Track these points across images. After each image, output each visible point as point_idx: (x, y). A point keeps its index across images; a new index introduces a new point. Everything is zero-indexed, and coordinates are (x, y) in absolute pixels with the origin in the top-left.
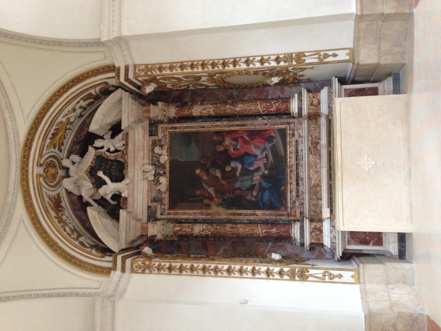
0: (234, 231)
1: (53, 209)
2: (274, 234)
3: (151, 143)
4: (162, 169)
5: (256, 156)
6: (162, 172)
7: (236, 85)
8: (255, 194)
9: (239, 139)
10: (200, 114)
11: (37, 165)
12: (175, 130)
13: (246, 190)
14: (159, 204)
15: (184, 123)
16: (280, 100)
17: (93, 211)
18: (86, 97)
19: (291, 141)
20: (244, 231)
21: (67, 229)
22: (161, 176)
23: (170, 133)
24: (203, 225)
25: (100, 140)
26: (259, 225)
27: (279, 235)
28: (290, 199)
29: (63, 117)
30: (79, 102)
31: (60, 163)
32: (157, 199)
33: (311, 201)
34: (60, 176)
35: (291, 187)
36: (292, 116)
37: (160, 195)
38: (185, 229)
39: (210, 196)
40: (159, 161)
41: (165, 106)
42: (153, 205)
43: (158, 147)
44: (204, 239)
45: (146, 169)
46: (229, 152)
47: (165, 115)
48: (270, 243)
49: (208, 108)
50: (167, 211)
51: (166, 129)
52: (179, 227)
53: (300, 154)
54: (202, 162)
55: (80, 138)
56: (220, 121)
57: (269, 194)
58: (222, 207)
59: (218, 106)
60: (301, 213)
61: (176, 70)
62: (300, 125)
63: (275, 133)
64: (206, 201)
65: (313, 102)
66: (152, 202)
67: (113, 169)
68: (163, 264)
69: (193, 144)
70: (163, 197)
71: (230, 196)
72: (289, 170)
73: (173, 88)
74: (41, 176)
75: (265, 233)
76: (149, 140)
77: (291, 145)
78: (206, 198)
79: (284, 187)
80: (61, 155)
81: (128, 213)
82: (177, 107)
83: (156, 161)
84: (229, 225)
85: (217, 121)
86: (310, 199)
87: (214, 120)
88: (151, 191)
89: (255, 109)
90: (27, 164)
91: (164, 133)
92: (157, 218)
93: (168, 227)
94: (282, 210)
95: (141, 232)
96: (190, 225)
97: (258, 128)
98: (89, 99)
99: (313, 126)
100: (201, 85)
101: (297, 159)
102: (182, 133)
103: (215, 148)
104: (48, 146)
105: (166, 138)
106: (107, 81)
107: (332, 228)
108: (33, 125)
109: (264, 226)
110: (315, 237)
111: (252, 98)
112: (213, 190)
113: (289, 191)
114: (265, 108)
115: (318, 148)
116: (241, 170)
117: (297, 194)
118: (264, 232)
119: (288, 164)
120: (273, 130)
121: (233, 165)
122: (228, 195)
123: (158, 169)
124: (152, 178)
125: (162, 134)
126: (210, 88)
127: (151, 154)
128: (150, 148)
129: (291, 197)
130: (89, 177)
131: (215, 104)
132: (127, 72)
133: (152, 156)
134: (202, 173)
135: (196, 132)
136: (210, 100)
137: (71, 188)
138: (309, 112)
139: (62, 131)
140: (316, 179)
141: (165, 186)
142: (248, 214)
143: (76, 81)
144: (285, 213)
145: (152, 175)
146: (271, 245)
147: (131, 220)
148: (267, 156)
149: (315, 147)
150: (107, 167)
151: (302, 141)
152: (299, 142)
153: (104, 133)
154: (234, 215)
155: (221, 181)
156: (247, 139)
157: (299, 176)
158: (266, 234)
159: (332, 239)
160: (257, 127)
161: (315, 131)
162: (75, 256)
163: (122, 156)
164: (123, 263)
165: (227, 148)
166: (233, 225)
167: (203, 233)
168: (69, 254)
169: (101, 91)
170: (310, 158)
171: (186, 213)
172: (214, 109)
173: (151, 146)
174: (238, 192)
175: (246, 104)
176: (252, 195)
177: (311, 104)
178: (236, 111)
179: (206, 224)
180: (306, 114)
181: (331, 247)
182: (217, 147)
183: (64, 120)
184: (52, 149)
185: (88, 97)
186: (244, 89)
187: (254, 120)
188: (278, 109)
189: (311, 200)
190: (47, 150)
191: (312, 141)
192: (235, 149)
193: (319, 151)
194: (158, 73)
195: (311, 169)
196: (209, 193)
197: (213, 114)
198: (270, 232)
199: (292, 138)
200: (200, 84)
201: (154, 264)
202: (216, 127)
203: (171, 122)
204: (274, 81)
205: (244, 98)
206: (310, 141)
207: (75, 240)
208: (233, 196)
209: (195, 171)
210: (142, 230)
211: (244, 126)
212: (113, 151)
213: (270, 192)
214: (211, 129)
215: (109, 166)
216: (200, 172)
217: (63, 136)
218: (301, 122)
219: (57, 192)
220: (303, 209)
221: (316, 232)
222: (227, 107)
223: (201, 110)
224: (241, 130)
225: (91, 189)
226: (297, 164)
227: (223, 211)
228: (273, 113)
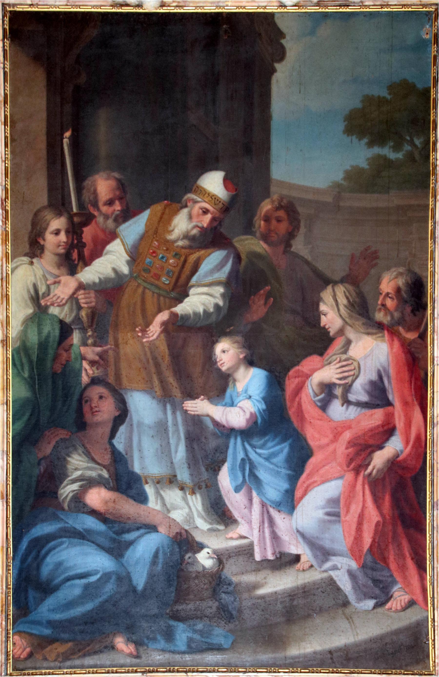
13: (112, 446)
39: (86, 252)
44: (408, 138)
46: (315, 359)
57: (96, 572)
63: (404, 609)
71: (85, 364)
103: (335, 283)
116: (216, 424)
121: (247, 379)
155: (164, 316)
182: (340, 290)
208: (85, 379)
209: (216, 169)
213: (106, 577)
216: (213, 198)
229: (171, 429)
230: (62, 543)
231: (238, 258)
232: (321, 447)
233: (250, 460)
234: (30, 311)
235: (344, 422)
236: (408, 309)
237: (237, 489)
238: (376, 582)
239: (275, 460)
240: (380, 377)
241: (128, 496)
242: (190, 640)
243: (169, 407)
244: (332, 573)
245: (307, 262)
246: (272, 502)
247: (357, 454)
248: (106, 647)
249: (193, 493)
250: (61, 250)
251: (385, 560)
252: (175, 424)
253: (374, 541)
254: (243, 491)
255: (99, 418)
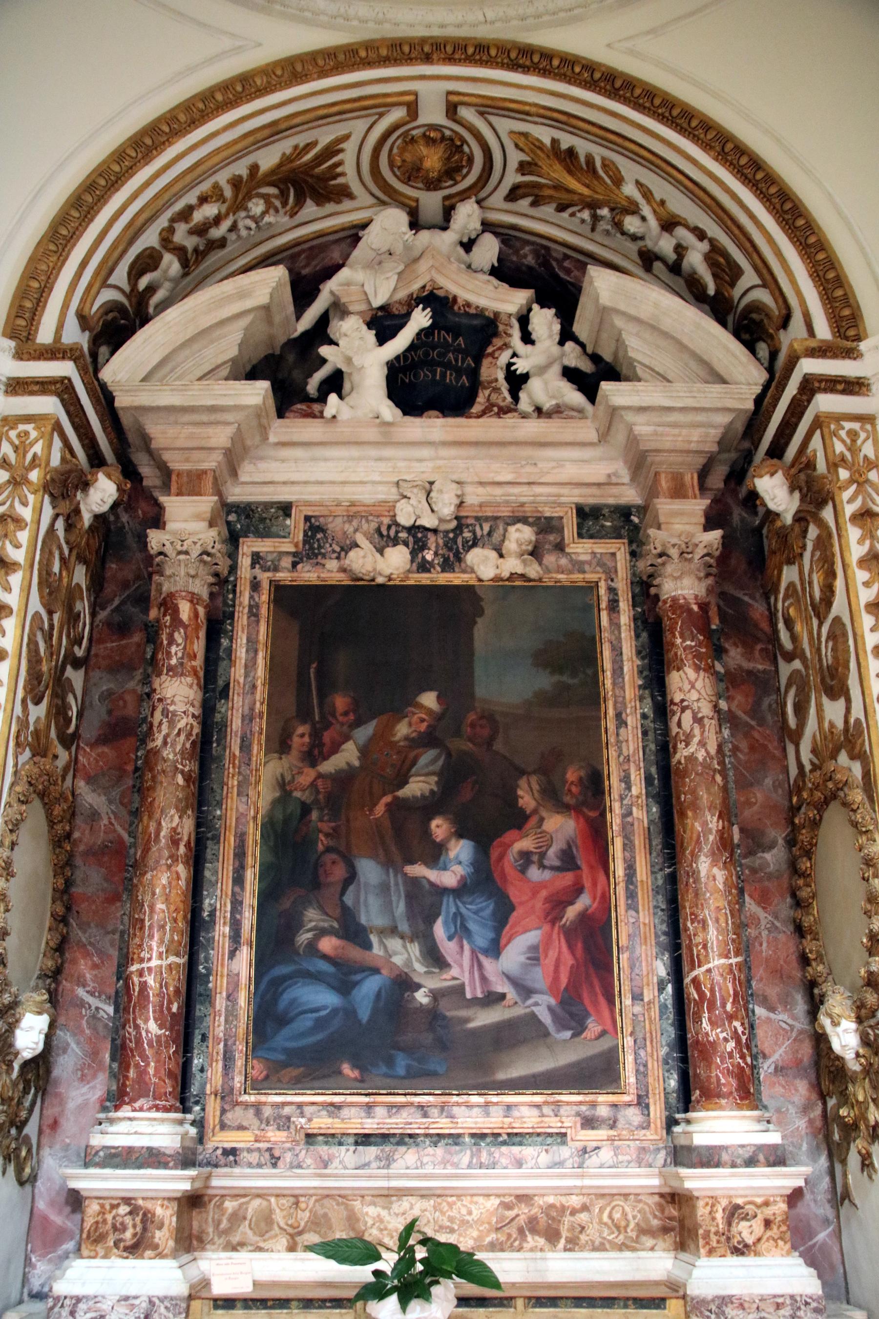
0: (161, 848)
1: (286, 160)
2: (137, 1027)
3: (548, 514)
4: (443, 556)
5: (495, 949)
6: (429, 556)
7: (810, 859)
8: (327, 944)
9: (568, 878)
10: (676, 704)
11: (449, 93)
12: (603, 605)
13: (342, 901)
14: (296, 545)
15: (634, 643)
16: (749, 1060)
17: (270, 290)
18: (721, 260)
19: (564, 1111)
20: (154, 894)
21: (210, 210)
22: (414, 554)
23: (592, 588)
24: (194, 716)
25: (557, 327)
26: (182, 960)
27: (132, 1051)
28: (300, 1106)
29: (638, 183)
30: (701, 235)
31: (463, 196)
32: (318, 540)
33: (283, 1201)
34: (417, 200)
35: (353, 1110)
36: (678, 1116)
37: (334, 551)
38: (180, 641)
39: (325, 750)
40: (475, 544)
41: (708, 555)
42: (295, 525)
43: (533, 538)
45: (441, 491)
47: (668, 556)
48: (110, 1010)
49: (702, 733)
50: (265, 577)
51: (611, 574)
52: (190, 619)
53: (502, 1154)
54: (472, 717)
55: (561, 267)
56: (648, 795)
57: (324, 1007)
58: (275, 803)
59: (713, 778)
60: (233, 1152)
61: (867, 584)
62: (634, 1156)
64: (301, 734)
65: (745, 1218)
66: (307, 519)
67: (443, 375)
68: (23, 536)
69: (545, 681)
70: (323, 561)
72: (431, 1099)
73: (781, 596)
74: (413, 109)
75: (144, 986)
76: (560, 505)
77: (546, 1110)
78: (316, 735)
79: (356, 1079)
80: (497, 199)
81: (258, 413)
82: (704, 607)
83: (474, 533)
84: (187, 827)
85: (649, 780)
86: (295, 1196)
87: (653, 770)
88: (350, 518)
89: (705, 947)
90: (455, 60)
91: (589, 563)
92: (241, 540)
93: (192, 572)
94: (253, 1068)
95: (179, 475)
96: (199, 662)
97: (622, 962)
98: (715, 276)
99: (630, 1217)
100: (801, 709)
101: (479, 1136)
102: (594, 638)
103: (529, 774)
104: (525, 135)
105: (571, 572)
106: (797, 320)
107: (144, 1305)
108: (603, 69)
109: (175, 981)
110: (109, 1217)
111: (752, 932)
112: (348, 764)
113: (337, 1099)
114: (712, 990)
115: (529, 1238)
116: (432, 884)
117: (320, 1138)
118: (145, 982)
119: (455, 1099)
120: (612, 1029)
122: (326, 827)
123: (441, 542)
124: (405, 520)
125: (587, 558)
126: (791, 749)
127: (505, 512)
128: (528, 510)
129: (308, 1110)
130: (412, 294)
131: (722, 763)
132: (840, 387)
133: (496, 518)
134: (424, 716)
135: (599, 694)
136: (735, 749)
137: (372, 238)
138: (698, 1198)
139: (585, 191)
140: (386, 1229)
141: (369, 568)
142: (241, 913)
143: (788, 206)
144: (238, 1080)
145: (418, 517)
146: (102, 1013)
147: (230, 430)
148: (493, 999)
149: (533, 1226)
150: (451, 355)
151: (560, 1164)
152: (555, 1148)
153: (583, 336)
154: (236, 855)
155: (388, 799)
156: (571, 912)
157: (402, 1149)
158: (137, 989)
159: (91, 1303)
160: (624, 957)
161: (605, 1224)
162: (91, 220)
163: (493, 405)
164: (43, 386)
165: (533, 821)
166: (188, 845)
167: (158, 715)
168: (102, 200)
169: (756, 307)
170: (481, 1199)
171: (256, 651)
172: (701, 759)
173: (539, 511)
174: (339, 872)
175: (729, 903)
176: (322, 932)
177: (734, 1212)
178: (695, 856)
179: (197, 730)
180: (688, 1185)
181: (57, 1299)
182: (534, 779)
183: (629, 190)
184: (515, 157)
185: (724, 271)
186: (794, 895)
187: (658, 944)
188: (707, 1050)
189: (292, 1200)
190: (512, 132)
191: (563, 1209)
192: (526, 857)
193: (517, 1243)
194: (849, 510)
195: (432, 1202)
196: (335, 749)
197: (678, 756)
198: (145, 1007)
199: (578, 1114)
200: (808, 701)
201: (25, 504)
202: (623, 774)
203: (637, 590)
204: (839, 1029)
205: (751, 896)
206: (563, 1200)
207: (164, 234)
208: (321, 847)
209: (431, 690)
210: (189, 473)
211: (627, 898)
212: (513, 368)
213: (335, 1011)
214: (613, 753)
215: (456, 360)
216: (429, 711)
217: (565, 197)
218: (649, 1158)
219: (356, 187)
220: (250, 1165)
221: (130, 1225)
222: (709, 818)
223: (695, 706)
224: (612, 886)
225: (369, 303)
226: (455, 1139)
227: (255, 804)
228: (690, 1024)
229: (393, 889)
230: (296, 983)
231: (449, 755)
232: (521, 903)
233: (461, 914)
234: (277, 794)
235: (540, 883)
236: (590, 794)
237: (450, 938)
238: (572, 1015)
239: (481, 914)
240: (569, 846)
241: (355, 943)
242: (408, 1067)
243: (391, 871)
244: (534, 1009)
245: (505, 757)
246: (480, 948)
247: (553, 909)
248: (334, 1072)
249: (412, 941)
250: (305, 749)
251: (580, 997)
252: (397, 884)
253: (569, 981)
254: (455, 940)
255: (331, 879)
